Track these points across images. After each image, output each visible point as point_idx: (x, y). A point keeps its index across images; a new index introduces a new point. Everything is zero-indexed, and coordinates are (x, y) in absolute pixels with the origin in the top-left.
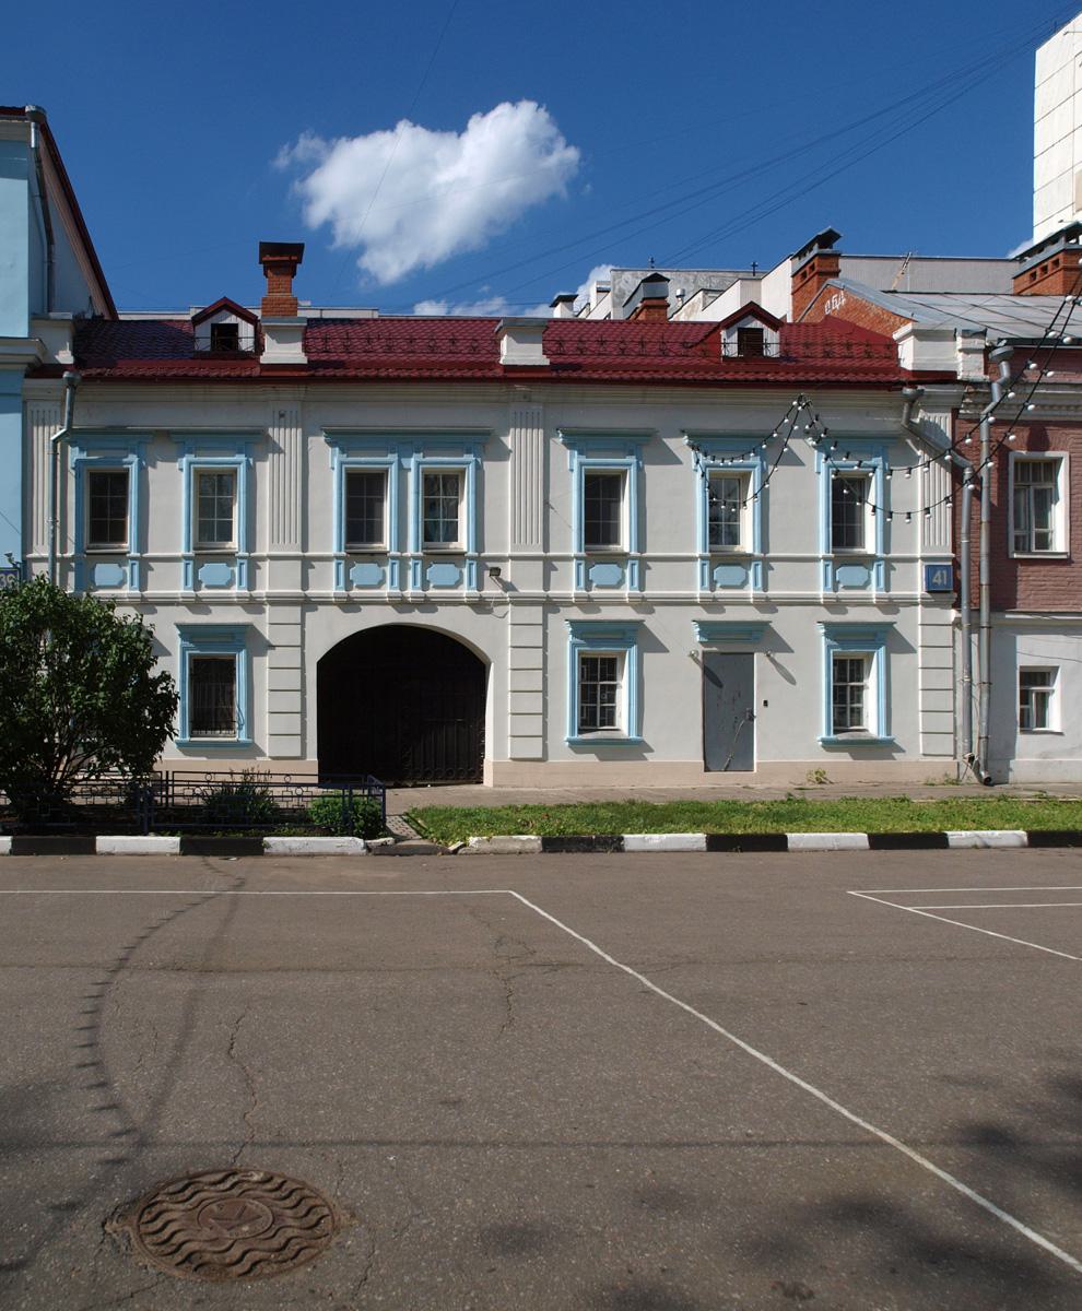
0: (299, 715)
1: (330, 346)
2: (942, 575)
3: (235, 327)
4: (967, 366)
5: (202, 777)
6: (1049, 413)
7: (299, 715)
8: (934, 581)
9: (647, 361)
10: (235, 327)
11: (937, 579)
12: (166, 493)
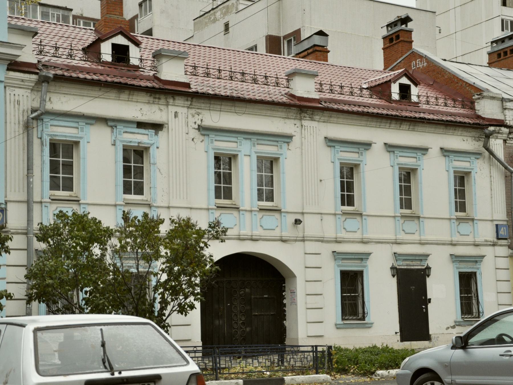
2: (504, 229)
8: (501, 233)
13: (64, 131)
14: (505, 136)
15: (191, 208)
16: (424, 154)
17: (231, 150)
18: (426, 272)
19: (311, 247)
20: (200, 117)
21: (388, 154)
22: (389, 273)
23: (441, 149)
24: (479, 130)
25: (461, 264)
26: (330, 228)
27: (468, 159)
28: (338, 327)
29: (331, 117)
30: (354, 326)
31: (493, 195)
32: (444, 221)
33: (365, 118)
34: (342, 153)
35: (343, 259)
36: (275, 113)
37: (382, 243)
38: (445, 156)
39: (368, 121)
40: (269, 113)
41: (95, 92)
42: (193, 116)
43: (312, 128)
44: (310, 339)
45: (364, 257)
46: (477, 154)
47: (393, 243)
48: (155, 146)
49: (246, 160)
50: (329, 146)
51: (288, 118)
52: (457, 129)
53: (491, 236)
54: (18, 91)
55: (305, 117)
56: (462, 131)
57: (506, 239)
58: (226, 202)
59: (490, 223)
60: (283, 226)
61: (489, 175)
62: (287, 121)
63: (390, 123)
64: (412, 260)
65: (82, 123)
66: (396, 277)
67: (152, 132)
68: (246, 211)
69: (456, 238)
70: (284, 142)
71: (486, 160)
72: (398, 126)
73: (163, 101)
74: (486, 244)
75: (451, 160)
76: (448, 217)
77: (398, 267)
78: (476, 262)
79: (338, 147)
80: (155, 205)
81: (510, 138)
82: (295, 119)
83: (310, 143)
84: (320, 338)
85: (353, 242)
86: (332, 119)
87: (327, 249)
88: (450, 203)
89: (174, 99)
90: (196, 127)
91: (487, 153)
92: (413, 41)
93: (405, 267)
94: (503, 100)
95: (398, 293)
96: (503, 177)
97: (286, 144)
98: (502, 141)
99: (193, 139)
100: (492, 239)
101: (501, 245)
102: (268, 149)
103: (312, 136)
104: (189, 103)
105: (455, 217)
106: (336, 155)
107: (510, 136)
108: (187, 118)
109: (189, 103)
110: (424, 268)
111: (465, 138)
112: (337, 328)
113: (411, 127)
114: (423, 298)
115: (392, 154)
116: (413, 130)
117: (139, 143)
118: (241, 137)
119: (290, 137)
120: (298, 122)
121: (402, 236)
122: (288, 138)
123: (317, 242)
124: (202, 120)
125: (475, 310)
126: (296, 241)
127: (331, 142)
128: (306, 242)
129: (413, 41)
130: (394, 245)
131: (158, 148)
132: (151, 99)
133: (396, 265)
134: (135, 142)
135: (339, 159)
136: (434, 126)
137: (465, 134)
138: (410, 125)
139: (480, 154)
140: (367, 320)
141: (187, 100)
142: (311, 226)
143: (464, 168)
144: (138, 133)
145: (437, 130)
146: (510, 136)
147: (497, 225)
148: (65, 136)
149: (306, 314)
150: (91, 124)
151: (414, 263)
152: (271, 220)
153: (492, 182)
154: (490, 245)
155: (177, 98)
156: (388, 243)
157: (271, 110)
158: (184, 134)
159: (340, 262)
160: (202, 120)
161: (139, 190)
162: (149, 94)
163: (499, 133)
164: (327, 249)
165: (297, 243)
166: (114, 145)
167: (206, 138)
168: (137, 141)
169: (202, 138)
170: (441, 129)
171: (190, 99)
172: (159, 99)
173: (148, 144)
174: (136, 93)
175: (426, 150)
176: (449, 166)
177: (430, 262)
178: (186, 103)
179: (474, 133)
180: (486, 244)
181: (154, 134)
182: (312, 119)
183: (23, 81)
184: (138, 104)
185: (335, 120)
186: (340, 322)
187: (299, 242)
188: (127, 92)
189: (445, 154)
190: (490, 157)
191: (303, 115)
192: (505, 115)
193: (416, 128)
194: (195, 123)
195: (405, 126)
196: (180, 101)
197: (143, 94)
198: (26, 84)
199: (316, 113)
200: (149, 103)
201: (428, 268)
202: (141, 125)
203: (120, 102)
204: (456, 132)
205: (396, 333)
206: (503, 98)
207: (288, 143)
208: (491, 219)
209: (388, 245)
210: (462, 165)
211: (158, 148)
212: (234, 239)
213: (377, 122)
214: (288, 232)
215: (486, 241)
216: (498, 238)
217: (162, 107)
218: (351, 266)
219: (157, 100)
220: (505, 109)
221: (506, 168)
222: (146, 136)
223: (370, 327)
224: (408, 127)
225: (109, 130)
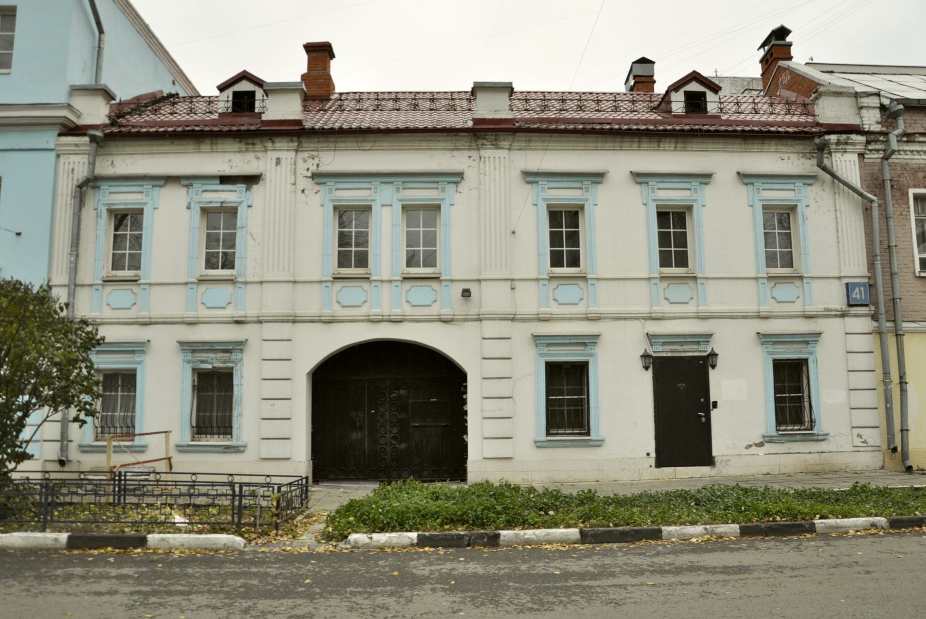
0: (59, 424)
1: (603, 105)
2: (860, 291)
3: (252, 94)
4: (871, 120)
5: (261, 480)
6: (917, 157)
7: (59, 424)
8: (854, 296)
9: (742, 116)
10: (252, 94)
11: (856, 295)
12: (172, 229)
13: (125, 198)
14: (860, 148)
15: (295, 282)
16: (706, 184)
17: (360, 200)
18: (710, 360)
19: (492, 329)
20: (316, 161)
21: (638, 187)
22: (639, 364)
23: (738, 173)
24: (808, 142)
25: (776, 346)
26: (528, 300)
27: (791, 187)
28: (539, 445)
29: (530, 141)
30: (568, 444)
31: (840, 239)
32: (746, 282)
33: (592, 138)
34: (550, 191)
35: (549, 345)
36: (433, 145)
37: (625, 319)
38: (746, 184)
39: (597, 142)
40: (424, 145)
41: (166, 147)
42: (305, 161)
43: (497, 159)
44: (489, 462)
45: (589, 341)
46: (808, 179)
47: (645, 319)
48: (244, 205)
49: (386, 211)
50: (528, 183)
51: (458, 149)
52: (767, 142)
53: (837, 301)
54: (74, 158)
55: (483, 144)
56: (776, 144)
57: (866, 305)
58: (680, 271)
59: (836, 282)
60: (447, 300)
61: (832, 209)
62: (456, 153)
63: (639, 142)
64: (682, 344)
65: (147, 186)
66: (650, 370)
67: (241, 187)
68: (382, 281)
69: (768, 307)
70: (449, 183)
71: (827, 187)
72: (656, 145)
73: (259, 147)
74: (828, 314)
75: (758, 189)
76: (754, 276)
77: (654, 355)
78: (807, 342)
79: (543, 182)
80: (239, 280)
81: (871, 151)
82: (469, 150)
83: (494, 181)
84: (506, 462)
85: (570, 319)
86: (533, 144)
87: (522, 332)
88: (757, 254)
89: (273, 142)
90: (309, 174)
91: (828, 177)
92: (654, 82)
93: (669, 355)
94: (857, 95)
95: (654, 391)
96: (860, 210)
97: (452, 186)
98: (856, 155)
99: (303, 191)
100: (838, 307)
101: (856, 316)
102: (421, 194)
103: (497, 170)
104: (296, 144)
105: (765, 275)
106: (541, 194)
107: (870, 147)
108: (295, 164)
109: (296, 144)
110: (705, 354)
111: (785, 156)
112: (538, 447)
113: (679, 145)
114: (702, 400)
115: (644, 186)
116: (685, 149)
117: (222, 203)
118: (376, 182)
119: (460, 175)
120: (474, 154)
121: (665, 308)
122: (457, 177)
123: (503, 322)
124: (318, 165)
125: (807, 418)
126: (465, 320)
127: (531, 177)
128: (483, 322)
129: (654, 82)
130: (649, 322)
131: (249, 206)
132: (243, 146)
133: (650, 352)
134: (217, 202)
135: (544, 200)
136: (721, 141)
137: (784, 149)
138: (676, 143)
139: (814, 177)
140: (593, 436)
141: (292, 141)
142: (491, 298)
143: (783, 200)
144: (223, 191)
145: (730, 147)
146: (870, 147)
147: (847, 284)
148: (126, 204)
149: (482, 426)
150: (160, 186)
151: (686, 347)
152: (422, 293)
153: (839, 220)
154: (836, 316)
155: (276, 140)
156: (636, 319)
157: (426, 140)
158: (289, 186)
159: (545, 350)
160: (318, 165)
161: (228, 263)
162: (237, 140)
163: (846, 143)
164: (522, 332)
165: (467, 323)
166: (188, 208)
167: (322, 188)
168: (219, 200)
169: (317, 188)
170: (737, 145)
171: (295, 139)
172: (254, 144)
173: (234, 202)
174: (220, 141)
175: (709, 176)
176: (753, 199)
177: (716, 345)
178: (291, 144)
179: (800, 147)
180: (828, 314)
181: (244, 189)
182: (497, 147)
183: (76, 145)
184: (226, 154)
185: (540, 144)
186: (543, 436)
187: (474, 323)
188: (208, 141)
189: (746, 181)
190: (833, 182)
191: (480, 142)
192: (862, 118)
193: (689, 146)
194: (308, 169)
195: (667, 144)
196: (282, 144)
197: (230, 141)
198: (81, 148)
199: (502, 138)
200: (240, 151)
201: (714, 355)
202: (225, 180)
203: (201, 155)
204: (766, 147)
205: (648, 454)
206: (856, 93)
207: (456, 183)
208: (837, 275)
209: (637, 322)
210: (780, 195)
211: (249, 206)
212: (362, 321)
213: (614, 142)
214: (455, 306)
215: (828, 310)
216: (850, 305)
217: (260, 155)
218: (566, 355)
219: (251, 146)
220: (861, 108)
221: (861, 195)
222: (234, 193)
223: (599, 446)
224: (673, 146)
225: (184, 190)
